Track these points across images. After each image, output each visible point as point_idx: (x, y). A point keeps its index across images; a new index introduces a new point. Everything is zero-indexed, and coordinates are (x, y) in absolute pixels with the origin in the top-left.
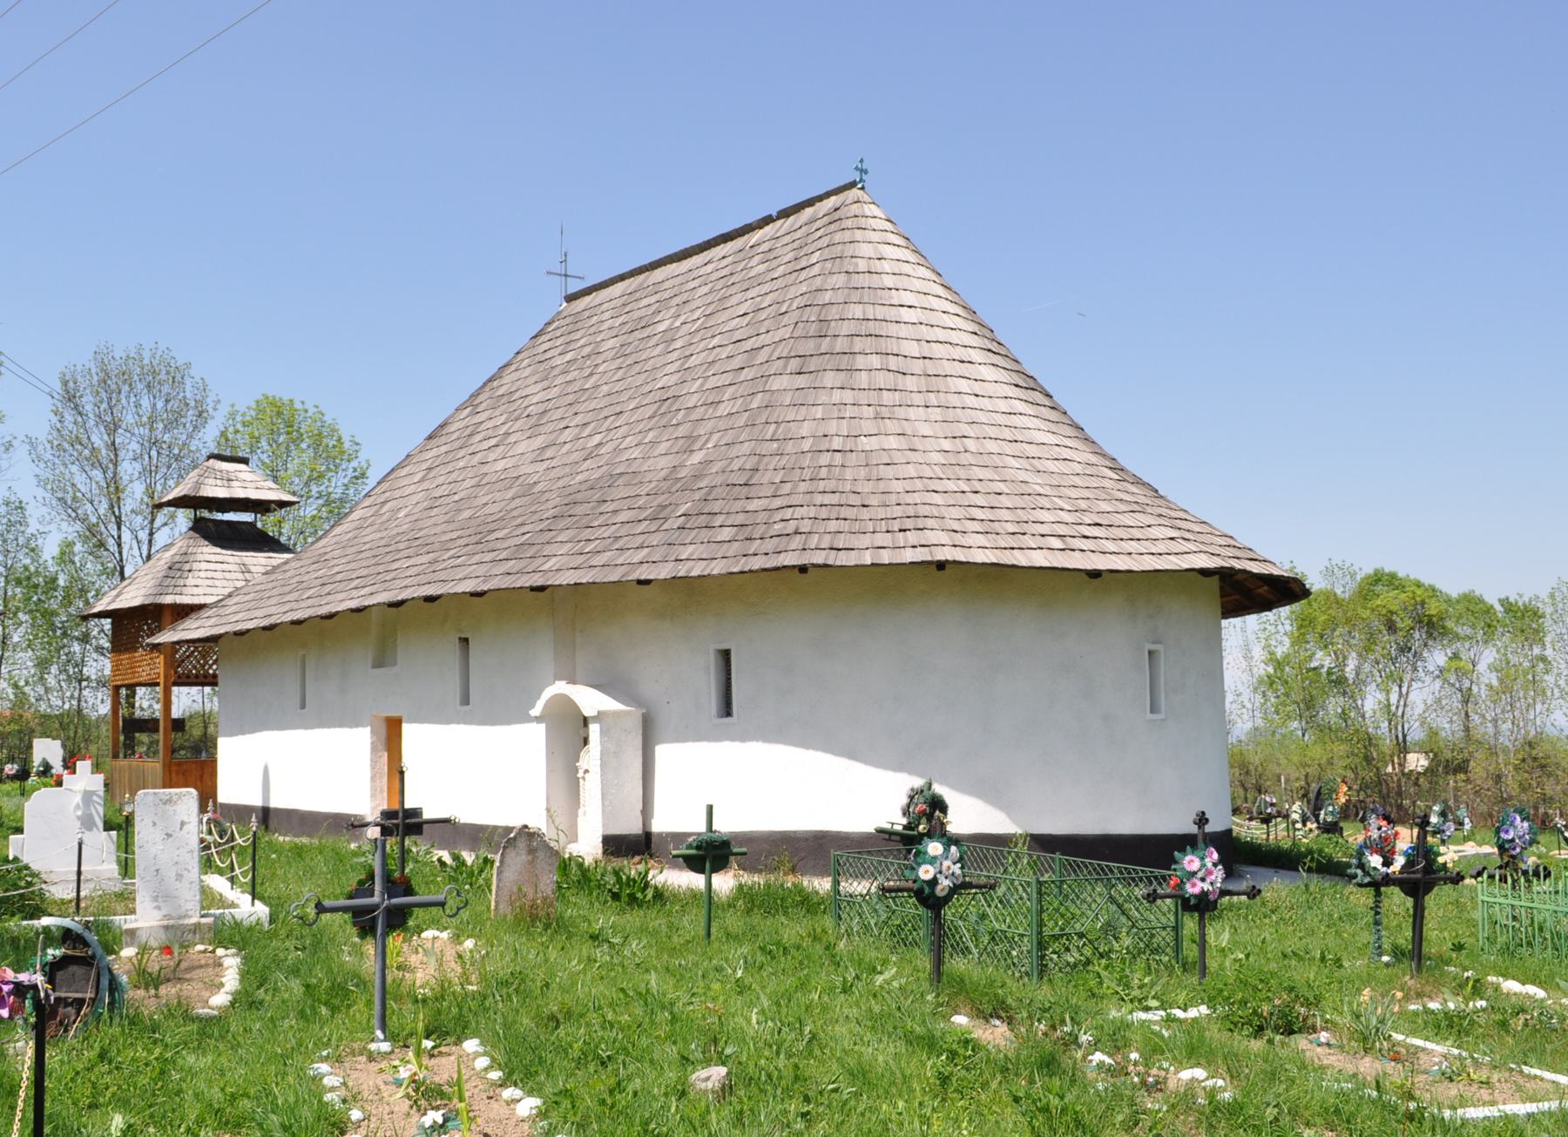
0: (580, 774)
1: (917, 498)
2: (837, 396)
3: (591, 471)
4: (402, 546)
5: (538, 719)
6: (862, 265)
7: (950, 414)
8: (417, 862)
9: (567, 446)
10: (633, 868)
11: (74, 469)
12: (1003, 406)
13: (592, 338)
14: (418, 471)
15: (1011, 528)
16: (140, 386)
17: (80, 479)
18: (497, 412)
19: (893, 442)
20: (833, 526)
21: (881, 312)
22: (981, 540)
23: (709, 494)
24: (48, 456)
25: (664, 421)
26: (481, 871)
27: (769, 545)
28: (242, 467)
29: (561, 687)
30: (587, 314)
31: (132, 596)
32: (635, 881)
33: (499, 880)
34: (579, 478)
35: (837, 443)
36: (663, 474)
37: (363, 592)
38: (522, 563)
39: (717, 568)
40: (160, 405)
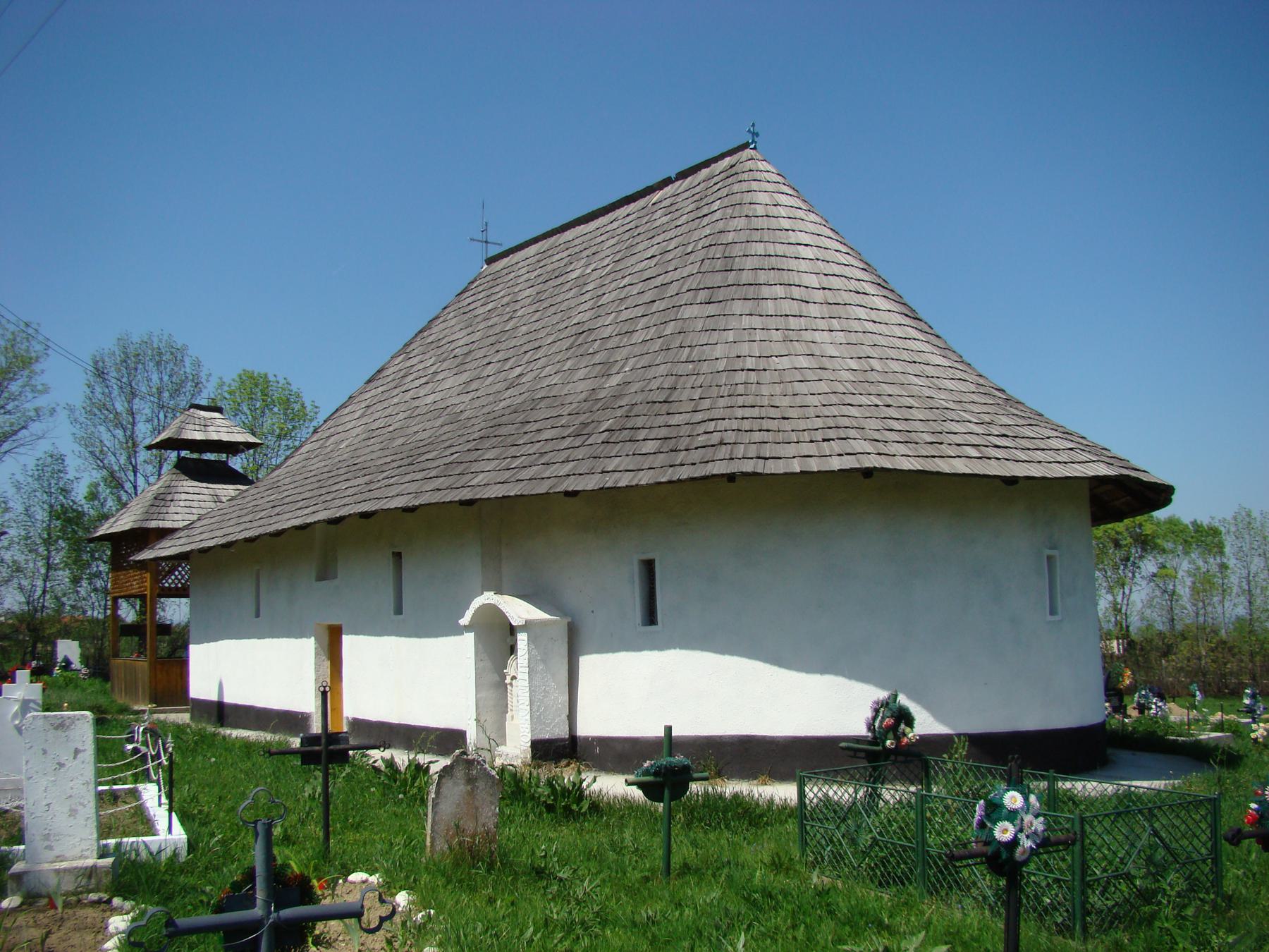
0: (508, 681)
1: (834, 411)
2: (746, 322)
3: (513, 398)
4: (342, 471)
5: (467, 628)
6: (760, 210)
7: (853, 338)
8: (353, 765)
9: (491, 379)
10: (568, 775)
11: (102, 429)
12: (898, 332)
13: (509, 290)
14: (357, 408)
15: (929, 438)
16: (151, 364)
17: (106, 437)
18: (427, 356)
19: (803, 362)
20: (757, 437)
21: (780, 249)
22: (902, 449)
23: (630, 411)
24: (82, 420)
25: (581, 351)
26: (414, 778)
27: (696, 456)
28: (217, 415)
29: (488, 597)
30: (505, 271)
31: (124, 522)
32: (569, 792)
33: (435, 813)
34: (502, 404)
35: (750, 363)
36: (583, 396)
37: (306, 511)
38: (452, 479)
39: (645, 478)
40: (166, 378)
